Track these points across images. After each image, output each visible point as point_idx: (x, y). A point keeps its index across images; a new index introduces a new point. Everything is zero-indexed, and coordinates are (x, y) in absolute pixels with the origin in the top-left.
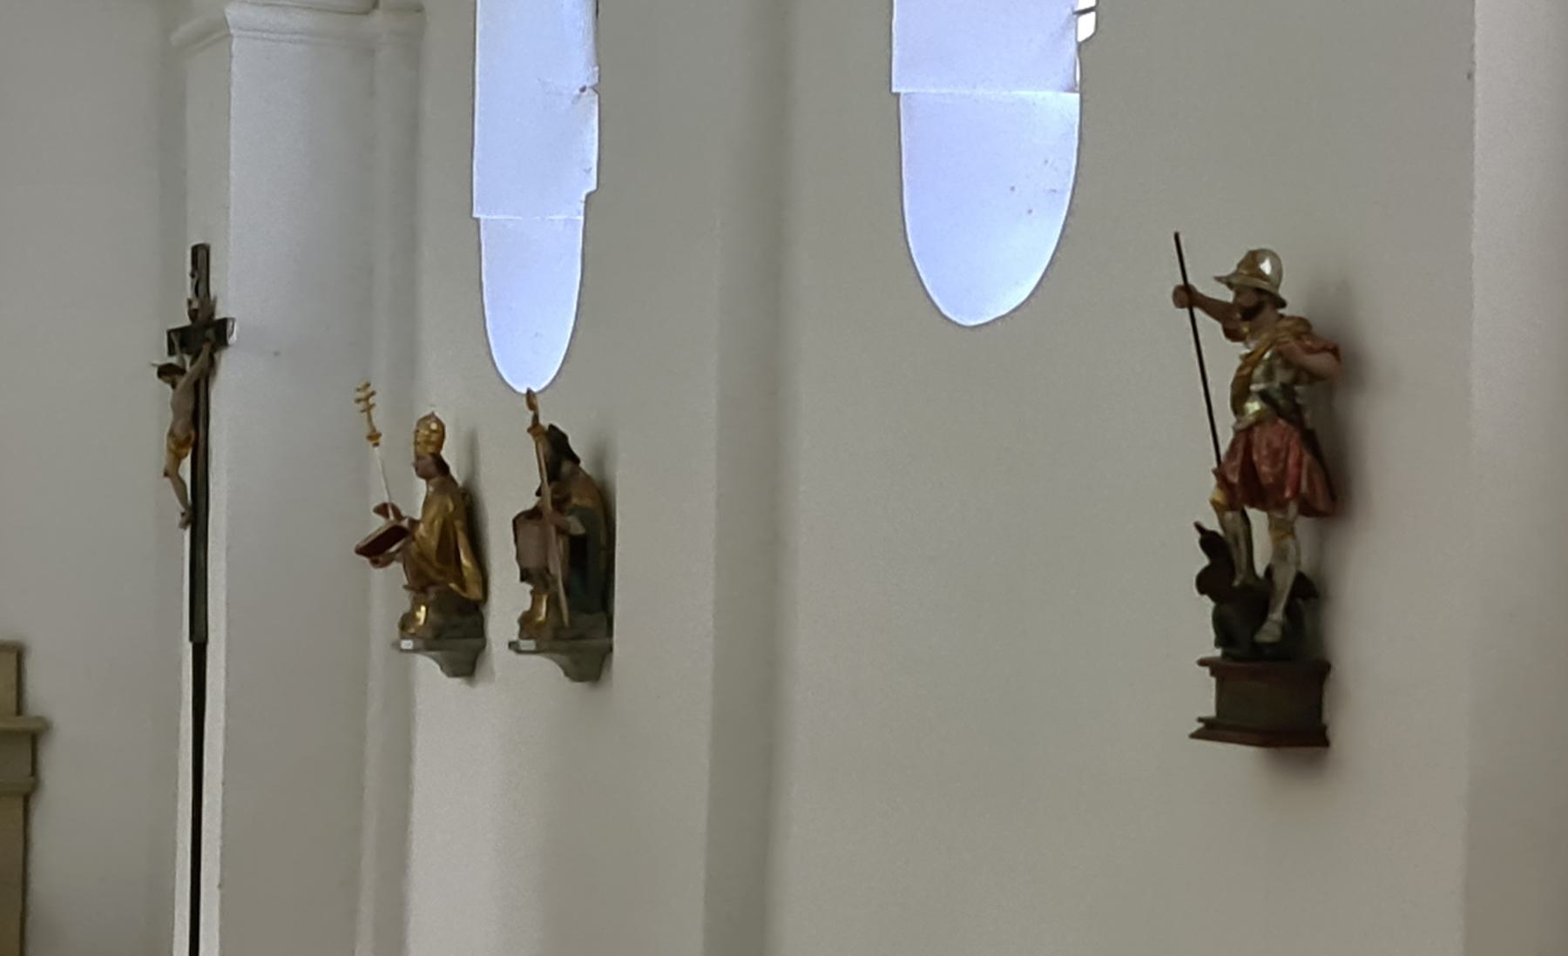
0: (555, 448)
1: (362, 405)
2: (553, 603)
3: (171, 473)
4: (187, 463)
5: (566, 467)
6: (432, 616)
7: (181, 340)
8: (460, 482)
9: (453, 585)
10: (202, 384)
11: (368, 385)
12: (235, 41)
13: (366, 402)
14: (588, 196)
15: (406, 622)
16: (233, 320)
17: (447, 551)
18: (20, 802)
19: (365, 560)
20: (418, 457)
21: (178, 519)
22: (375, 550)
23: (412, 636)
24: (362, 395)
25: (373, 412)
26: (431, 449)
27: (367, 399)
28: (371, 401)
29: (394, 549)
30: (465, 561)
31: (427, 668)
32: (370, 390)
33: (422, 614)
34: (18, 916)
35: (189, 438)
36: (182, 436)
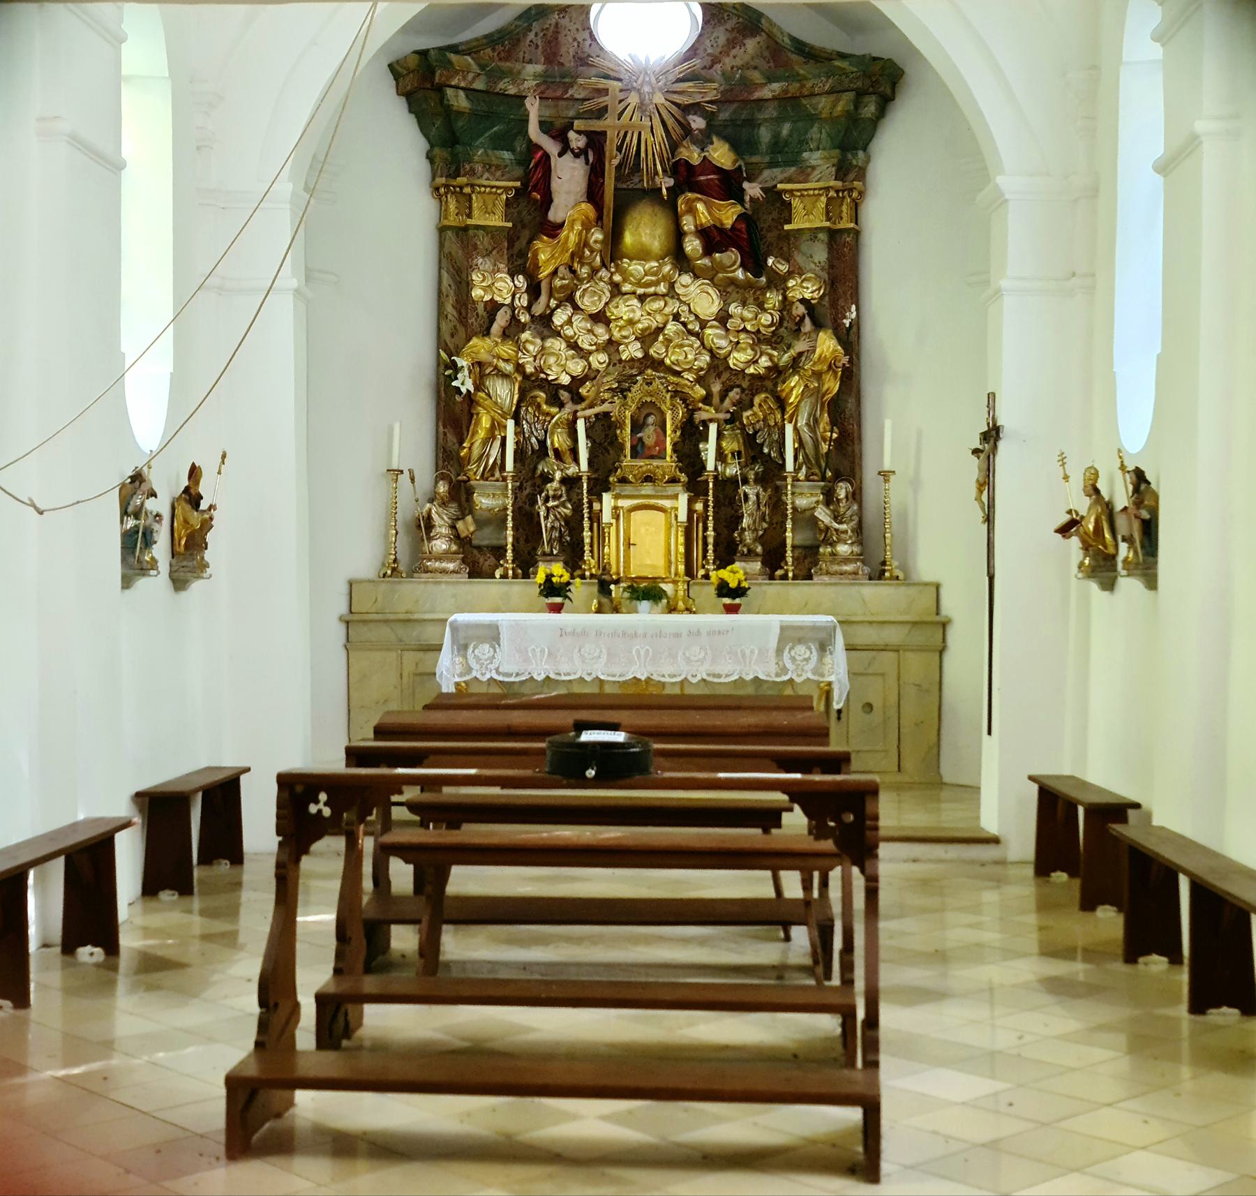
0: (1139, 476)
1: (1061, 462)
2: (1136, 553)
3: (978, 499)
4: (985, 493)
5: (1143, 487)
6: (1092, 562)
7: (985, 437)
8: (1107, 499)
9: (1100, 547)
10: (991, 456)
11: (1063, 453)
12: (1008, 301)
13: (1063, 461)
14: (1158, 355)
15: (1081, 565)
16: (1003, 426)
17: (1098, 529)
18: (938, 654)
19: (1059, 536)
20: (1085, 486)
21: (982, 519)
22: (1064, 530)
23: (1082, 571)
24: (1060, 458)
25: (1066, 466)
26: (1091, 482)
27: (1063, 459)
28: (1064, 461)
29: (1072, 530)
30: (1107, 535)
31: (1093, 587)
32: (1064, 456)
33: (1087, 561)
34: (937, 709)
35: (985, 482)
36: (981, 480)
